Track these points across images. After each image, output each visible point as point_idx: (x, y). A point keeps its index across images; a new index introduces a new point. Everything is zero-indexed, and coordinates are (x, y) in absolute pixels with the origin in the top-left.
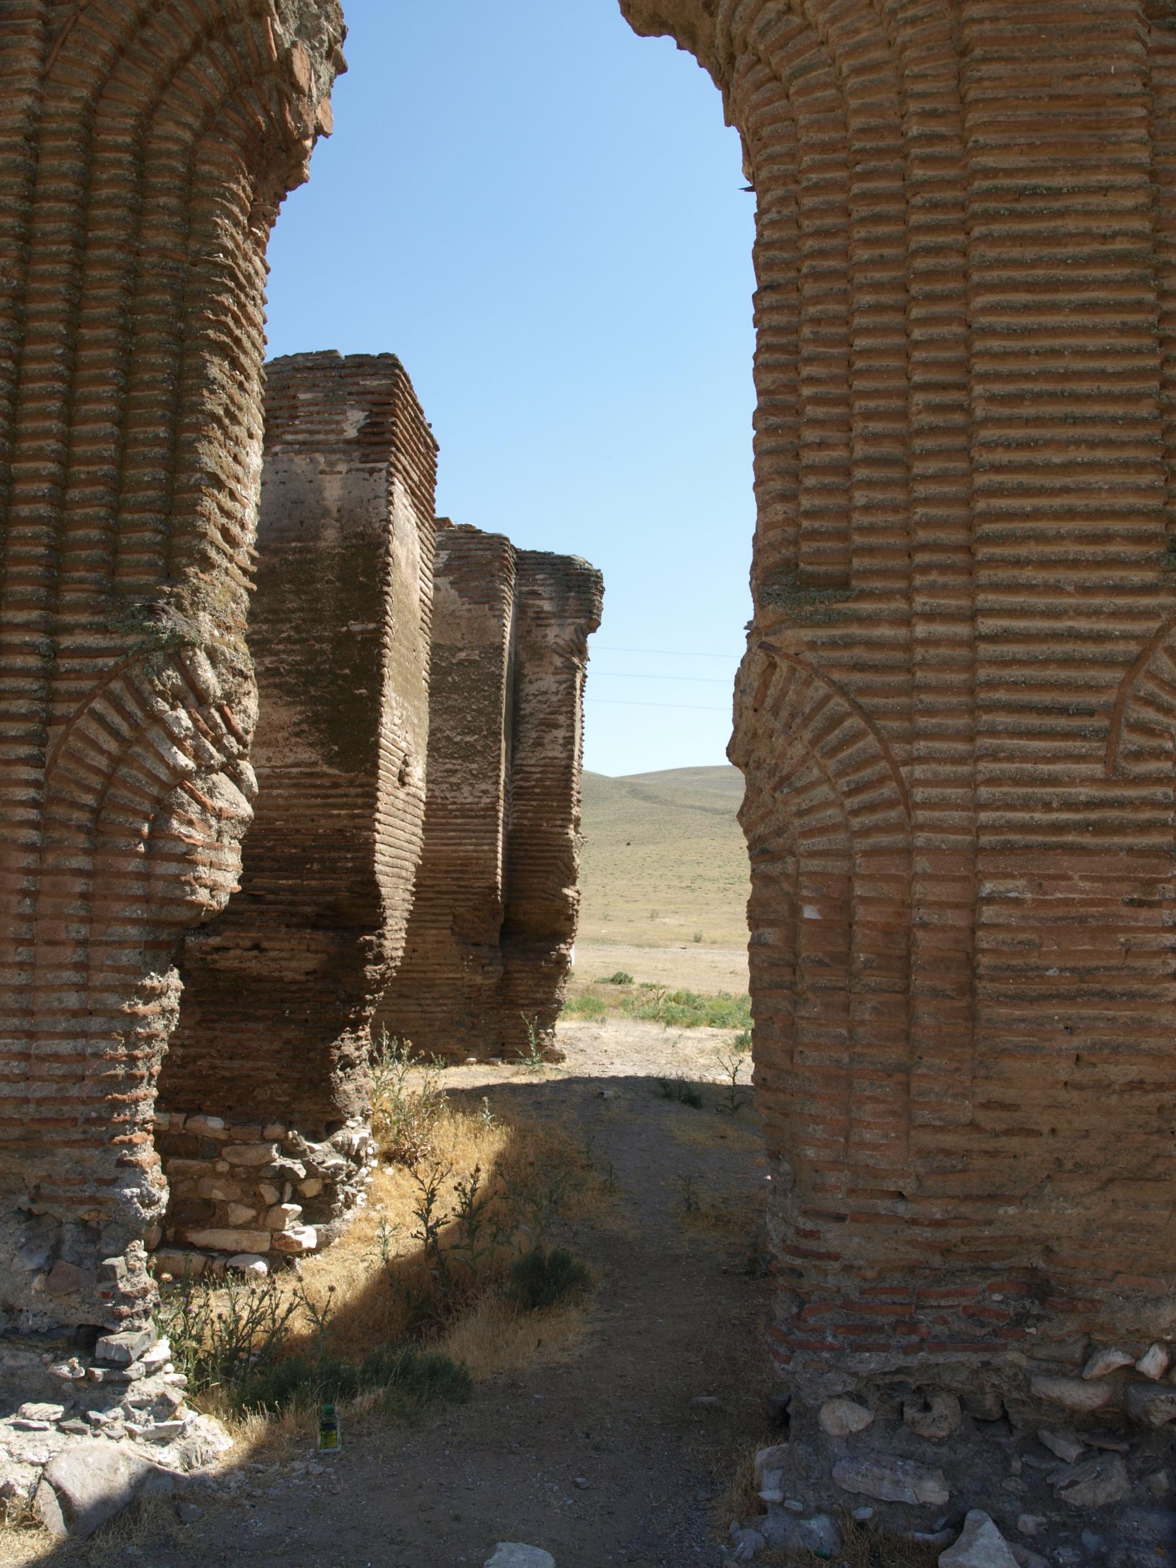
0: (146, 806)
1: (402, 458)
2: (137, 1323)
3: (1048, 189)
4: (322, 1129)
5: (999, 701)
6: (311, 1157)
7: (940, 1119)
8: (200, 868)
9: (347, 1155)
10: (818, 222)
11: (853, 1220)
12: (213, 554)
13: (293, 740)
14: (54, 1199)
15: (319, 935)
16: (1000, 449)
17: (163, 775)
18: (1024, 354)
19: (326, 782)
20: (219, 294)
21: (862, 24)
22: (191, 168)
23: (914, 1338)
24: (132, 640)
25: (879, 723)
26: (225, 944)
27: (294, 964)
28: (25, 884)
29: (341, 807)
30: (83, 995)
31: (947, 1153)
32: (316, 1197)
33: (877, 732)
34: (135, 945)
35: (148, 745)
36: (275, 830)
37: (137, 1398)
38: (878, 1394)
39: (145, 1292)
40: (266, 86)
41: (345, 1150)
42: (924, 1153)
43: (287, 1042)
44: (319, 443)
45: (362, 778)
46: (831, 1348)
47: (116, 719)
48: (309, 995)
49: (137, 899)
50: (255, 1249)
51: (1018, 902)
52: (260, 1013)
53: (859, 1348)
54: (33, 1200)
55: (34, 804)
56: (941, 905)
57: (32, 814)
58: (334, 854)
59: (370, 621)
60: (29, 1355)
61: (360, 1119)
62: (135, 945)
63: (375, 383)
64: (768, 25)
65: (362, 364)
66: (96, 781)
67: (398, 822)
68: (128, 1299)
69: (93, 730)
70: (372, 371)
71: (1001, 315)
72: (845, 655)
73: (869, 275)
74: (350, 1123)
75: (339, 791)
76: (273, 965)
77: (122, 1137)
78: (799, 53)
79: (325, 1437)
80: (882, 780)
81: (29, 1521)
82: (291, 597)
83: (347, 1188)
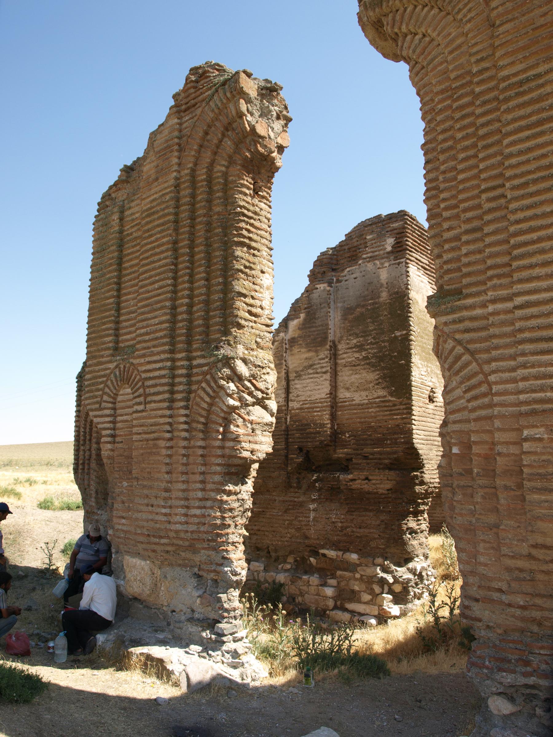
0: (220, 421)
1: (414, 255)
2: (231, 621)
3: (534, 76)
4: (402, 561)
5: (526, 338)
6: (396, 574)
7: (513, 552)
8: (243, 443)
9: (415, 574)
10: (443, 127)
11: (483, 602)
12: (243, 322)
13: (376, 387)
14: (203, 570)
15: (392, 473)
16: (519, 212)
17: (225, 409)
18: (528, 161)
19: (391, 404)
20: (238, 223)
21: (452, 30)
22: (226, 180)
23: (529, 669)
24: (212, 359)
25: (477, 356)
26: (354, 478)
27: (382, 486)
28: (184, 452)
29: (397, 415)
30: (204, 493)
31: (521, 570)
32: (400, 592)
33: (476, 360)
34: (220, 473)
35: (220, 398)
36: (371, 427)
37: (227, 649)
38: (523, 698)
39: (234, 610)
40: (247, 142)
41: (413, 571)
42: (509, 569)
43: (382, 521)
44: (376, 256)
45: (405, 401)
46: (487, 668)
47: (208, 390)
48: (390, 500)
49: (219, 456)
50: (372, 614)
51: (540, 440)
52: (371, 508)
53: (500, 670)
54: (199, 570)
55: (186, 423)
56: (507, 443)
57: (185, 427)
58: (396, 436)
59: (404, 330)
60: (196, 628)
61: (422, 558)
62: (220, 473)
63: (397, 225)
64: (416, 47)
65: (391, 217)
66: (204, 413)
67: (429, 420)
68: (227, 611)
69: (202, 394)
70: (395, 220)
71: (515, 145)
72: (461, 326)
73: (462, 144)
74: (416, 559)
75: (397, 407)
76: (374, 487)
77: (223, 548)
78: (429, 53)
79: (306, 680)
80: (480, 384)
81: (176, 684)
82: (371, 325)
83: (416, 590)
